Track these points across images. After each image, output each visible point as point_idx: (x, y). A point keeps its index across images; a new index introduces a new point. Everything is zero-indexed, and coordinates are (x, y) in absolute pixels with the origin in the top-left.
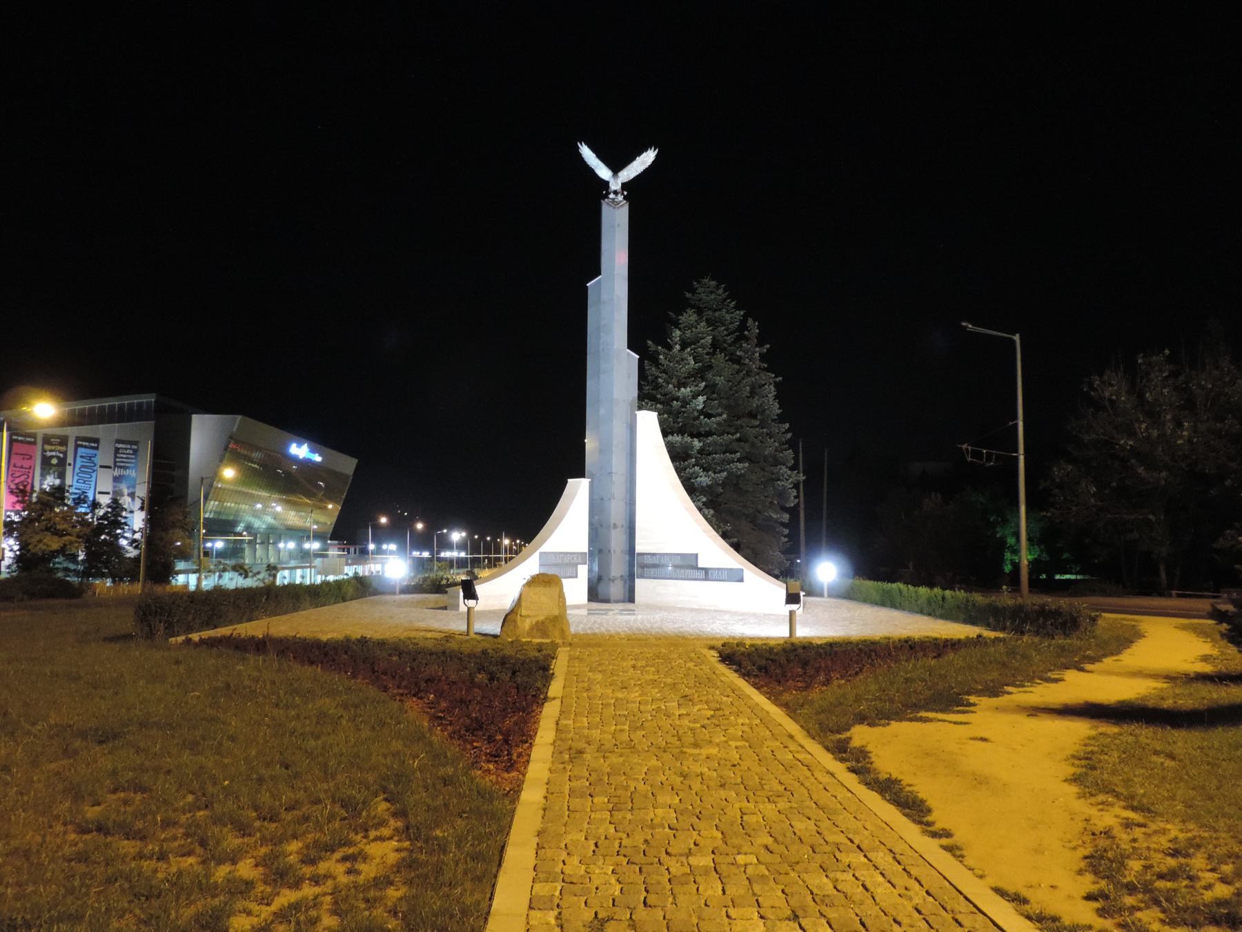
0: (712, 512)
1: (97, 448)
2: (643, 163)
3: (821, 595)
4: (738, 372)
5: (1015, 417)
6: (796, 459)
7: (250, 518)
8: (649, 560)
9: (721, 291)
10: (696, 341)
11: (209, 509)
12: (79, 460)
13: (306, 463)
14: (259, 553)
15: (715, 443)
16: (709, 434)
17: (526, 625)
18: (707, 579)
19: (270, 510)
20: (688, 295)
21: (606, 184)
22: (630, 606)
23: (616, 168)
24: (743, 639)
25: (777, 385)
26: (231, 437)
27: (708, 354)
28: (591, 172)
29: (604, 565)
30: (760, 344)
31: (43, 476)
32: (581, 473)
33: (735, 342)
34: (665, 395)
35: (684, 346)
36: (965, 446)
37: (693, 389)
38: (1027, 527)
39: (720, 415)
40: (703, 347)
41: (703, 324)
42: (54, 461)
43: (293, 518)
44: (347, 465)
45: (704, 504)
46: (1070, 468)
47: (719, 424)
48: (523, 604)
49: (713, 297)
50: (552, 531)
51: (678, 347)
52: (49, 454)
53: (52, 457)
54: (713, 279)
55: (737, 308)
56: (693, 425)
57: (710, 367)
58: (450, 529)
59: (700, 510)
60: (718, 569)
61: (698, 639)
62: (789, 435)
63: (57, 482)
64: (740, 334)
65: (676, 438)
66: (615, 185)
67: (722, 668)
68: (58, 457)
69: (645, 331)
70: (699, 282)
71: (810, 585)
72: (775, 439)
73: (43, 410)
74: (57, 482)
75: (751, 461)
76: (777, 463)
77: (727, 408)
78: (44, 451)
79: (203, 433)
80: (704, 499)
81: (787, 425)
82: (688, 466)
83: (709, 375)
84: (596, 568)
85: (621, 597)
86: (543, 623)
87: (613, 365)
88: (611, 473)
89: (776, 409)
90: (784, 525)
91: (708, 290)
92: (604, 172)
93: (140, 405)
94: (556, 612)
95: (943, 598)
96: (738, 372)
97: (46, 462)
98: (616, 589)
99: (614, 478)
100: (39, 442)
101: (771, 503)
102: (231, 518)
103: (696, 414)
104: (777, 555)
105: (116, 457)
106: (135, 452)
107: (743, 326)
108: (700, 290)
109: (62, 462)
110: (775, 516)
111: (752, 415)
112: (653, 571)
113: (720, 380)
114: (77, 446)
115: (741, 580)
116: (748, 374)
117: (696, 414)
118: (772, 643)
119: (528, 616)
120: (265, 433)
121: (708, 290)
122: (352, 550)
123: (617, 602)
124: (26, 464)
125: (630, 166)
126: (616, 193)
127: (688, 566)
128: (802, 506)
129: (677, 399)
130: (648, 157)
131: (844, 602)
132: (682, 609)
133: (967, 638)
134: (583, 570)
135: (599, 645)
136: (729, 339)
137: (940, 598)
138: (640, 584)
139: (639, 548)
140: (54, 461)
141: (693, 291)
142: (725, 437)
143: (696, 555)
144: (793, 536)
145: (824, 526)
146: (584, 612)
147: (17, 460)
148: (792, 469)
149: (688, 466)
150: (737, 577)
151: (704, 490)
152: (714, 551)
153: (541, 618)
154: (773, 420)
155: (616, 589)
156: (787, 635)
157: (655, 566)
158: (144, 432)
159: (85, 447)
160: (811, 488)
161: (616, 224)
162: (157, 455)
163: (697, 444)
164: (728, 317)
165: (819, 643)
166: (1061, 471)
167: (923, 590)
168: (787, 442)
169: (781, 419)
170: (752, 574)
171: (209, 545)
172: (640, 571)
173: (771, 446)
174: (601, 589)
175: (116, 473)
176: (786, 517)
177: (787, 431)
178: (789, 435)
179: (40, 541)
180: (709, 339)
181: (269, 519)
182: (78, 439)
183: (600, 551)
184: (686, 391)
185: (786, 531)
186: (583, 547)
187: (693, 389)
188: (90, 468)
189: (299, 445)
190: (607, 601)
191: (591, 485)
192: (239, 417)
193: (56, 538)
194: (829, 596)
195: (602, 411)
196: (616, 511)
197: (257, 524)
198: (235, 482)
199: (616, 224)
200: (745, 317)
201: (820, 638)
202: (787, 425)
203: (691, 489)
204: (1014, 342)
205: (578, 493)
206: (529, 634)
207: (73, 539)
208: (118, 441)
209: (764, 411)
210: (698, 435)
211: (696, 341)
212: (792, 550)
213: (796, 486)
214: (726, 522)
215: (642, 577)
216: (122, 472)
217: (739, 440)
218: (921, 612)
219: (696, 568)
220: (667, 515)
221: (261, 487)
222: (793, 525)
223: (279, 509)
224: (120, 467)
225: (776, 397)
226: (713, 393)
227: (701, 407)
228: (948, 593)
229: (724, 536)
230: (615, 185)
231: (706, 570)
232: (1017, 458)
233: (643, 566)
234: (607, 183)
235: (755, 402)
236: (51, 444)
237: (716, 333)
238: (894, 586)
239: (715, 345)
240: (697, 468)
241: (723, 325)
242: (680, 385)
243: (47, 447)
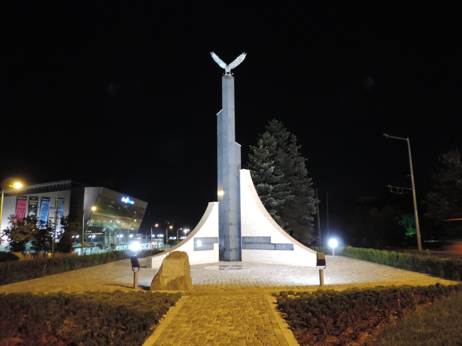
0: (279, 217)
1: (49, 201)
2: (240, 60)
3: (332, 254)
4: (288, 156)
5: (410, 173)
6: (315, 193)
7: (108, 226)
8: (247, 240)
9: (280, 124)
10: (269, 145)
11: (91, 223)
12: (42, 206)
13: (128, 204)
14: (110, 239)
15: (280, 187)
16: (277, 183)
17: (165, 282)
18: (275, 249)
19: (115, 223)
20: (267, 127)
21: (223, 70)
22: (239, 263)
23: (228, 63)
24: (293, 287)
25: (306, 162)
26: (99, 196)
27: (275, 150)
28: (217, 65)
29: (227, 243)
30: (298, 145)
31: (29, 212)
33: (287, 145)
34: (257, 167)
35: (264, 146)
36: (389, 186)
37: (269, 164)
38: (419, 220)
39: (281, 175)
40: (273, 146)
41: (273, 137)
42: (33, 206)
43: (124, 225)
44: (144, 205)
45: (276, 214)
46: (435, 194)
47: (281, 178)
48: (164, 270)
49: (277, 126)
50: (200, 227)
51: (262, 146)
52: (31, 204)
53: (32, 205)
54: (276, 120)
55: (287, 131)
56: (270, 180)
57: (276, 155)
58: (184, 228)
59: (272, 216)
60: (281, 244)
61: (266, 288)
62: (312, 183)
63: (34, 214)
64: (289, 141)
65: (262, 185)
66: (228, 70)
67: (278, 317)
68: (35, 205)
69: (245, 135)
70: (271, 121)
71: (326, 250)
72: (306, 186)
73: (18, 185)
74: (34, 214)
75: (296, 195)
76: (307, 195)
77: (284, 172)
78: (29, 202)
79: (89, 194)
80: (276, 212)
81: (311, 179)
82: (268, 197)
83: (276, 158)
84: (223, 244)
85: (235, 258)
86: (175, 281)
87: (230, 150)
89: (306, 172)
90: (312, 222)
91: (275, 124)
92: (222, 65)
93: (62, 185)
94: (183, 274)
95: (397, 256)
96: (288, 156)
97: (30, 206)
99: (230, 201)
100: (28, 199)
101: (306, 213)
102: (99, 226)
103: (271, 175)
104: (310, 236)
106: (63, 202)
107: (290, 138)
108: (271, 124)
109: (36, 207)
110: (307, 218)
111: (295, 175)
113: (281, 160)
114: (42, 201)
115: (292, 249)
116: (293, 157)
117: (271, 175)
118: (310, 291)
119: (167, 277)
120: (112, 193)
121: (275, 124)
122: (146, 237)
124: (23, 208)
125: (234, 62)
126: (228, 73)
127: (265, 243)
128: (318, 215)
129: (262, 168)
130: (242, 58)
131: (343, 257)
132: (263, 265)
133: (430, 286)
134: (216, 246)
135: (205, 294)
136: (284, 144)
137: (395, 257)
138: (244, 252)
139: (243, 235)
140: (33, 206)
141: (268, 125)
142: (284, 184)
143: (270, 237)
144: (316, 227)
145: (328, 222)
146: (217, 268)
147: (19, 206)
148: (314, 198)
149: (268, 197)
150: (290, 248)
151: (276, 208)
152: (279, 235)
153: (174, 278)
154: (305, 177)
155: (233, 255)
156: (318, 283)
157: (250, 243)
158: (67, 194)
159: (45, 201)
160: (321, 206)
161: (228, 87)
163: (271, 187)
164: (283, 135)
165: (340, 290)
166: (431, 196)
167: (385, 252)
168: (312, 186)
169: (308, 176)
170: (298, 246)
171: (90, 237)
172: (244, 245)
173: (304, 189)
174: (225, 254)
176: (312, 219)
177: (311, 182)
178: (312, 183)
179: (17, 237)
180: (275, 143)
181: (115, 226)
182: (42, 198)
183: (225, 236)
184: (265, 165)
185: (313, 225)
186: (217, 235)
187: (269, 164)
188: (46, 208)
189: (125, 198)
190: (228, 260)
192: (102, 188)
193: (23, 236)
194: (336, 254)
195: (224, 171)
196: (232, 217)
197: (111, 228)
198: (98, 211)
199: (228, 87)
200: (291, 134)
201: (339, 286)
202: (311, 179)
203: (268, 207)
204: (406, 142)
205: (213, 209)
206: (167, 288)
207: (30, 236)
209: (301, 173)
210: (272, 184)
211: (269, 145)
212: (315, 233)
213: (316, 205)
214: (286, 221)
215: (244, 248)
217: (290, 185)
218: (385, 264)
219: (270, 243)
220: (256, 218)
221: (112, 214)
222: (315, 222)
223: (119, 222)
225: (306, 167)
226: (278, 166)
227: (272, 171)
228: (400, 254)
229: (285, 228)
230: (228, 70)
231: (275, 245)
232: (412, 191)
233: (245, 243)
234: (224, 69)
235: (297, 169)
236: (32, 200)
237: (278, 141)
238: (369, 250)
239: (278, 146)
240: (272, 198)
241: (281, 138)
242: (263, 162)
243: (31, 201)
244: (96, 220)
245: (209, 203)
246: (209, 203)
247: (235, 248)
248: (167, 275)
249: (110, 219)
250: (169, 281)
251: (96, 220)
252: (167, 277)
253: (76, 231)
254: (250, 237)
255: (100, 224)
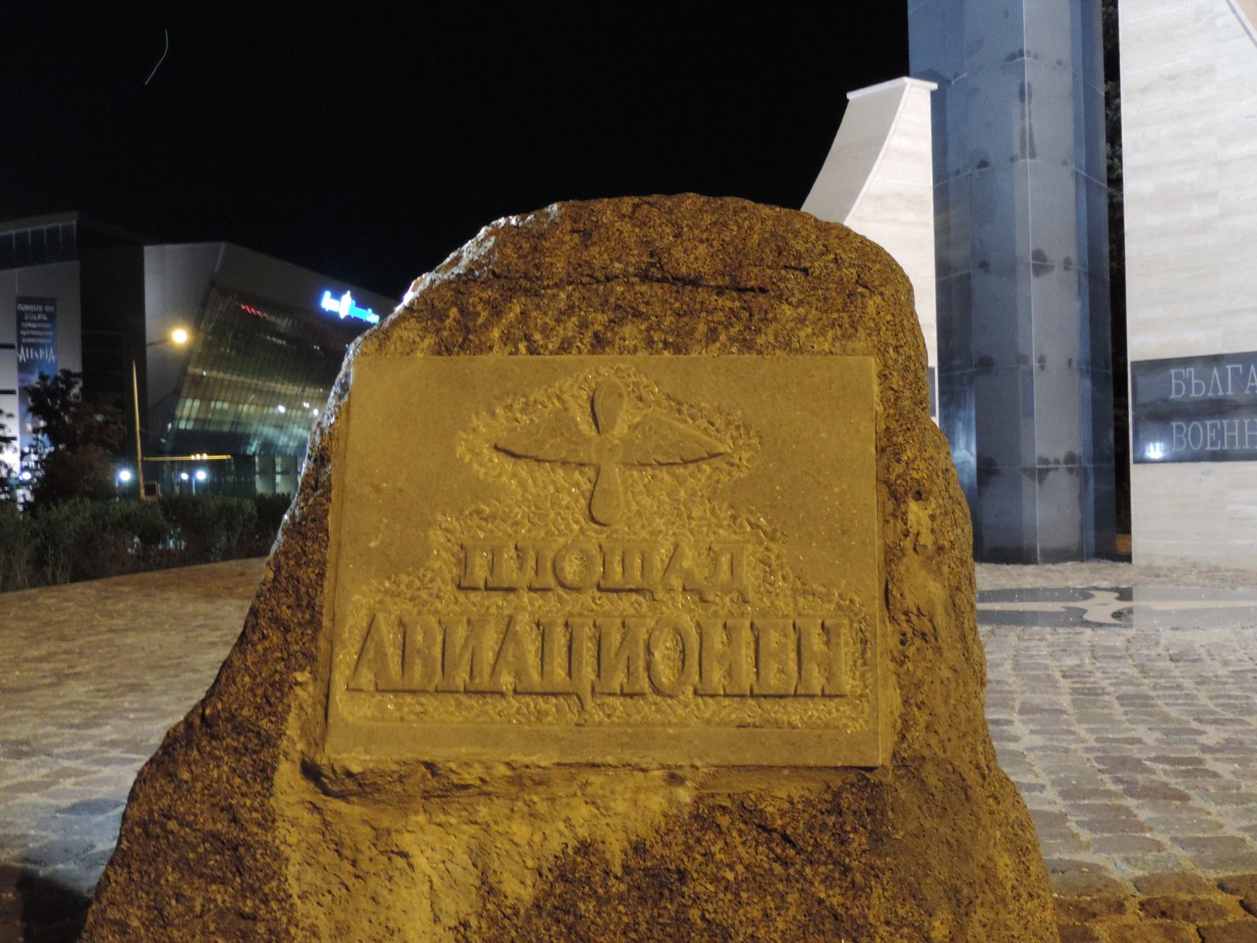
7: (269, 431)
8: (1193, 388)
32: (891, 62)
79: (162, 273)
86: (655, 878)
88: (1016, 56)
93: (37, 235)
94: (858, 720)
98: (1053, 508)
102: (226, 428)
105: (19, 328)
106: (51, 317)
112: (1207, 428)
119: (439, 787)
123: (1057, 556)
139: (1142, 344)
153: (626, 812)
162: (88, 321)
175: (23, 356)
189: (337, 295)
191: (939, 102)
192: (223, 246)
196: (1043, 206)
208: (23, 300)
216: (32, 354)
224: (28, 345)
244: (206, 399)
245: (851, 96)
246: (851, 96)
247: (1071, 459)
248: (444, 731)
249: (277, 398)
250: (518, 888)
251: (206, 399)
252: (439, 787)
253: (107, 445)
254: (1216, 360)
255: (230, 418)
